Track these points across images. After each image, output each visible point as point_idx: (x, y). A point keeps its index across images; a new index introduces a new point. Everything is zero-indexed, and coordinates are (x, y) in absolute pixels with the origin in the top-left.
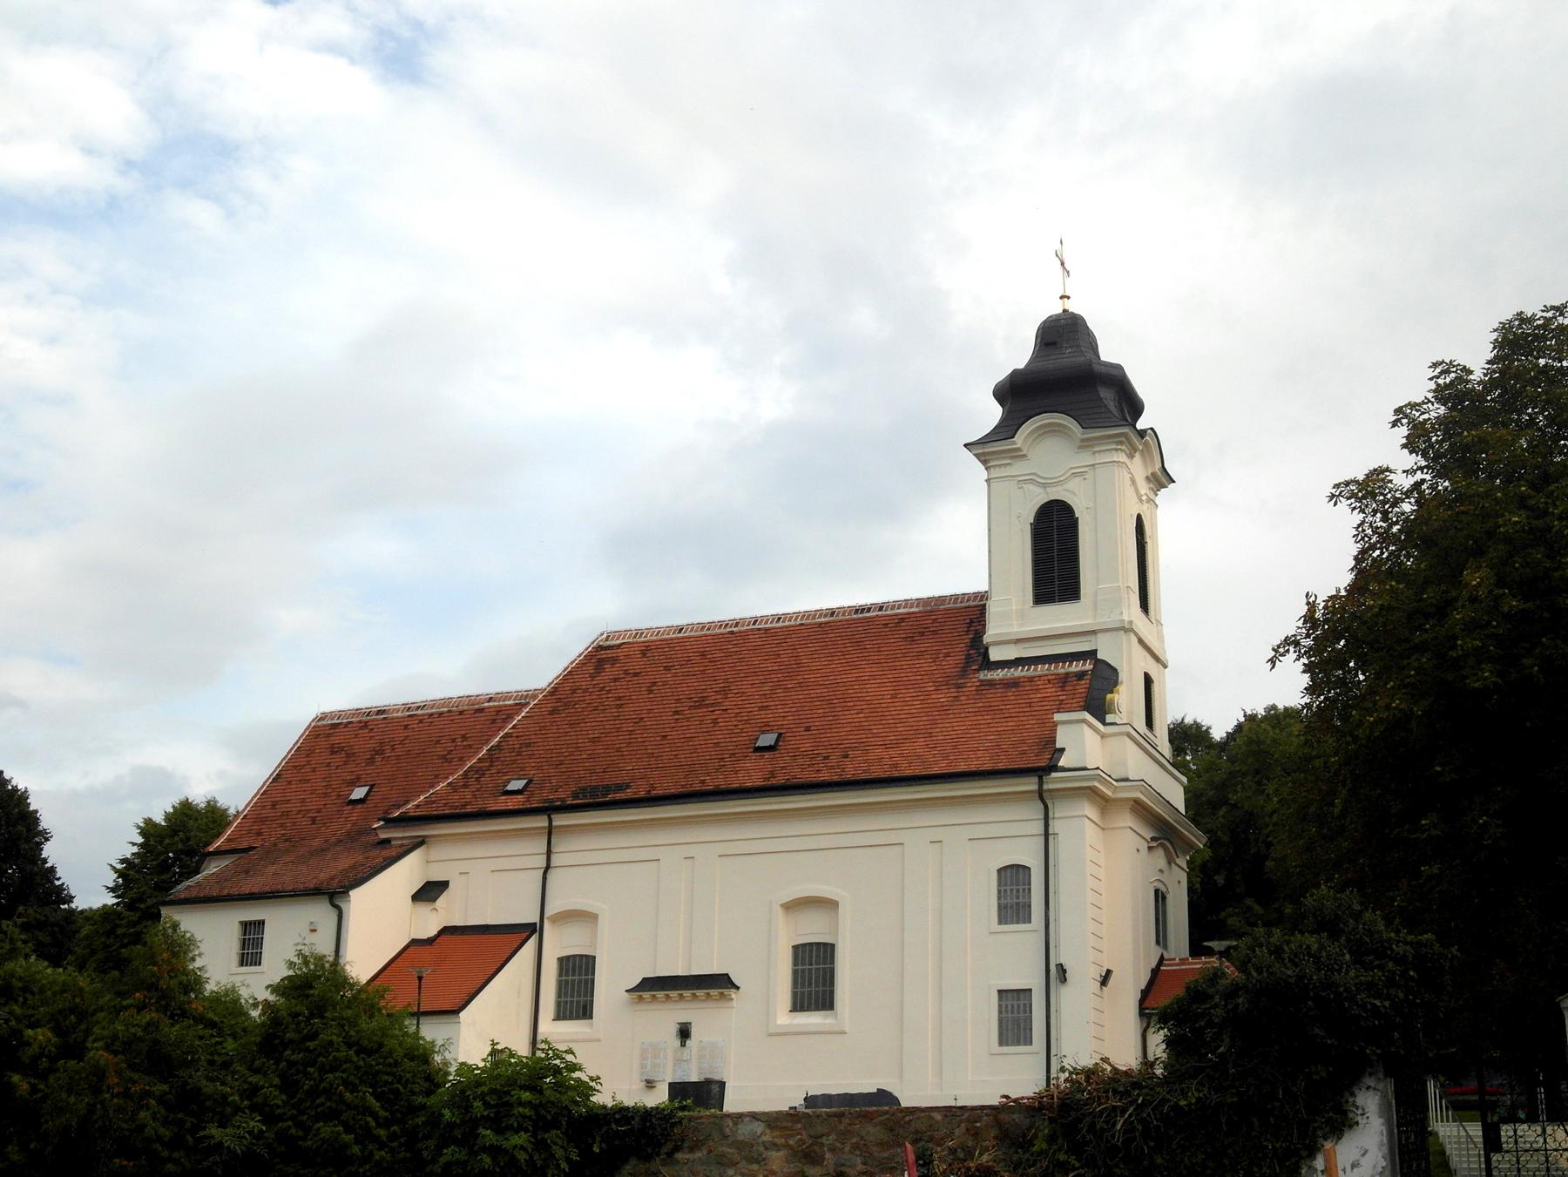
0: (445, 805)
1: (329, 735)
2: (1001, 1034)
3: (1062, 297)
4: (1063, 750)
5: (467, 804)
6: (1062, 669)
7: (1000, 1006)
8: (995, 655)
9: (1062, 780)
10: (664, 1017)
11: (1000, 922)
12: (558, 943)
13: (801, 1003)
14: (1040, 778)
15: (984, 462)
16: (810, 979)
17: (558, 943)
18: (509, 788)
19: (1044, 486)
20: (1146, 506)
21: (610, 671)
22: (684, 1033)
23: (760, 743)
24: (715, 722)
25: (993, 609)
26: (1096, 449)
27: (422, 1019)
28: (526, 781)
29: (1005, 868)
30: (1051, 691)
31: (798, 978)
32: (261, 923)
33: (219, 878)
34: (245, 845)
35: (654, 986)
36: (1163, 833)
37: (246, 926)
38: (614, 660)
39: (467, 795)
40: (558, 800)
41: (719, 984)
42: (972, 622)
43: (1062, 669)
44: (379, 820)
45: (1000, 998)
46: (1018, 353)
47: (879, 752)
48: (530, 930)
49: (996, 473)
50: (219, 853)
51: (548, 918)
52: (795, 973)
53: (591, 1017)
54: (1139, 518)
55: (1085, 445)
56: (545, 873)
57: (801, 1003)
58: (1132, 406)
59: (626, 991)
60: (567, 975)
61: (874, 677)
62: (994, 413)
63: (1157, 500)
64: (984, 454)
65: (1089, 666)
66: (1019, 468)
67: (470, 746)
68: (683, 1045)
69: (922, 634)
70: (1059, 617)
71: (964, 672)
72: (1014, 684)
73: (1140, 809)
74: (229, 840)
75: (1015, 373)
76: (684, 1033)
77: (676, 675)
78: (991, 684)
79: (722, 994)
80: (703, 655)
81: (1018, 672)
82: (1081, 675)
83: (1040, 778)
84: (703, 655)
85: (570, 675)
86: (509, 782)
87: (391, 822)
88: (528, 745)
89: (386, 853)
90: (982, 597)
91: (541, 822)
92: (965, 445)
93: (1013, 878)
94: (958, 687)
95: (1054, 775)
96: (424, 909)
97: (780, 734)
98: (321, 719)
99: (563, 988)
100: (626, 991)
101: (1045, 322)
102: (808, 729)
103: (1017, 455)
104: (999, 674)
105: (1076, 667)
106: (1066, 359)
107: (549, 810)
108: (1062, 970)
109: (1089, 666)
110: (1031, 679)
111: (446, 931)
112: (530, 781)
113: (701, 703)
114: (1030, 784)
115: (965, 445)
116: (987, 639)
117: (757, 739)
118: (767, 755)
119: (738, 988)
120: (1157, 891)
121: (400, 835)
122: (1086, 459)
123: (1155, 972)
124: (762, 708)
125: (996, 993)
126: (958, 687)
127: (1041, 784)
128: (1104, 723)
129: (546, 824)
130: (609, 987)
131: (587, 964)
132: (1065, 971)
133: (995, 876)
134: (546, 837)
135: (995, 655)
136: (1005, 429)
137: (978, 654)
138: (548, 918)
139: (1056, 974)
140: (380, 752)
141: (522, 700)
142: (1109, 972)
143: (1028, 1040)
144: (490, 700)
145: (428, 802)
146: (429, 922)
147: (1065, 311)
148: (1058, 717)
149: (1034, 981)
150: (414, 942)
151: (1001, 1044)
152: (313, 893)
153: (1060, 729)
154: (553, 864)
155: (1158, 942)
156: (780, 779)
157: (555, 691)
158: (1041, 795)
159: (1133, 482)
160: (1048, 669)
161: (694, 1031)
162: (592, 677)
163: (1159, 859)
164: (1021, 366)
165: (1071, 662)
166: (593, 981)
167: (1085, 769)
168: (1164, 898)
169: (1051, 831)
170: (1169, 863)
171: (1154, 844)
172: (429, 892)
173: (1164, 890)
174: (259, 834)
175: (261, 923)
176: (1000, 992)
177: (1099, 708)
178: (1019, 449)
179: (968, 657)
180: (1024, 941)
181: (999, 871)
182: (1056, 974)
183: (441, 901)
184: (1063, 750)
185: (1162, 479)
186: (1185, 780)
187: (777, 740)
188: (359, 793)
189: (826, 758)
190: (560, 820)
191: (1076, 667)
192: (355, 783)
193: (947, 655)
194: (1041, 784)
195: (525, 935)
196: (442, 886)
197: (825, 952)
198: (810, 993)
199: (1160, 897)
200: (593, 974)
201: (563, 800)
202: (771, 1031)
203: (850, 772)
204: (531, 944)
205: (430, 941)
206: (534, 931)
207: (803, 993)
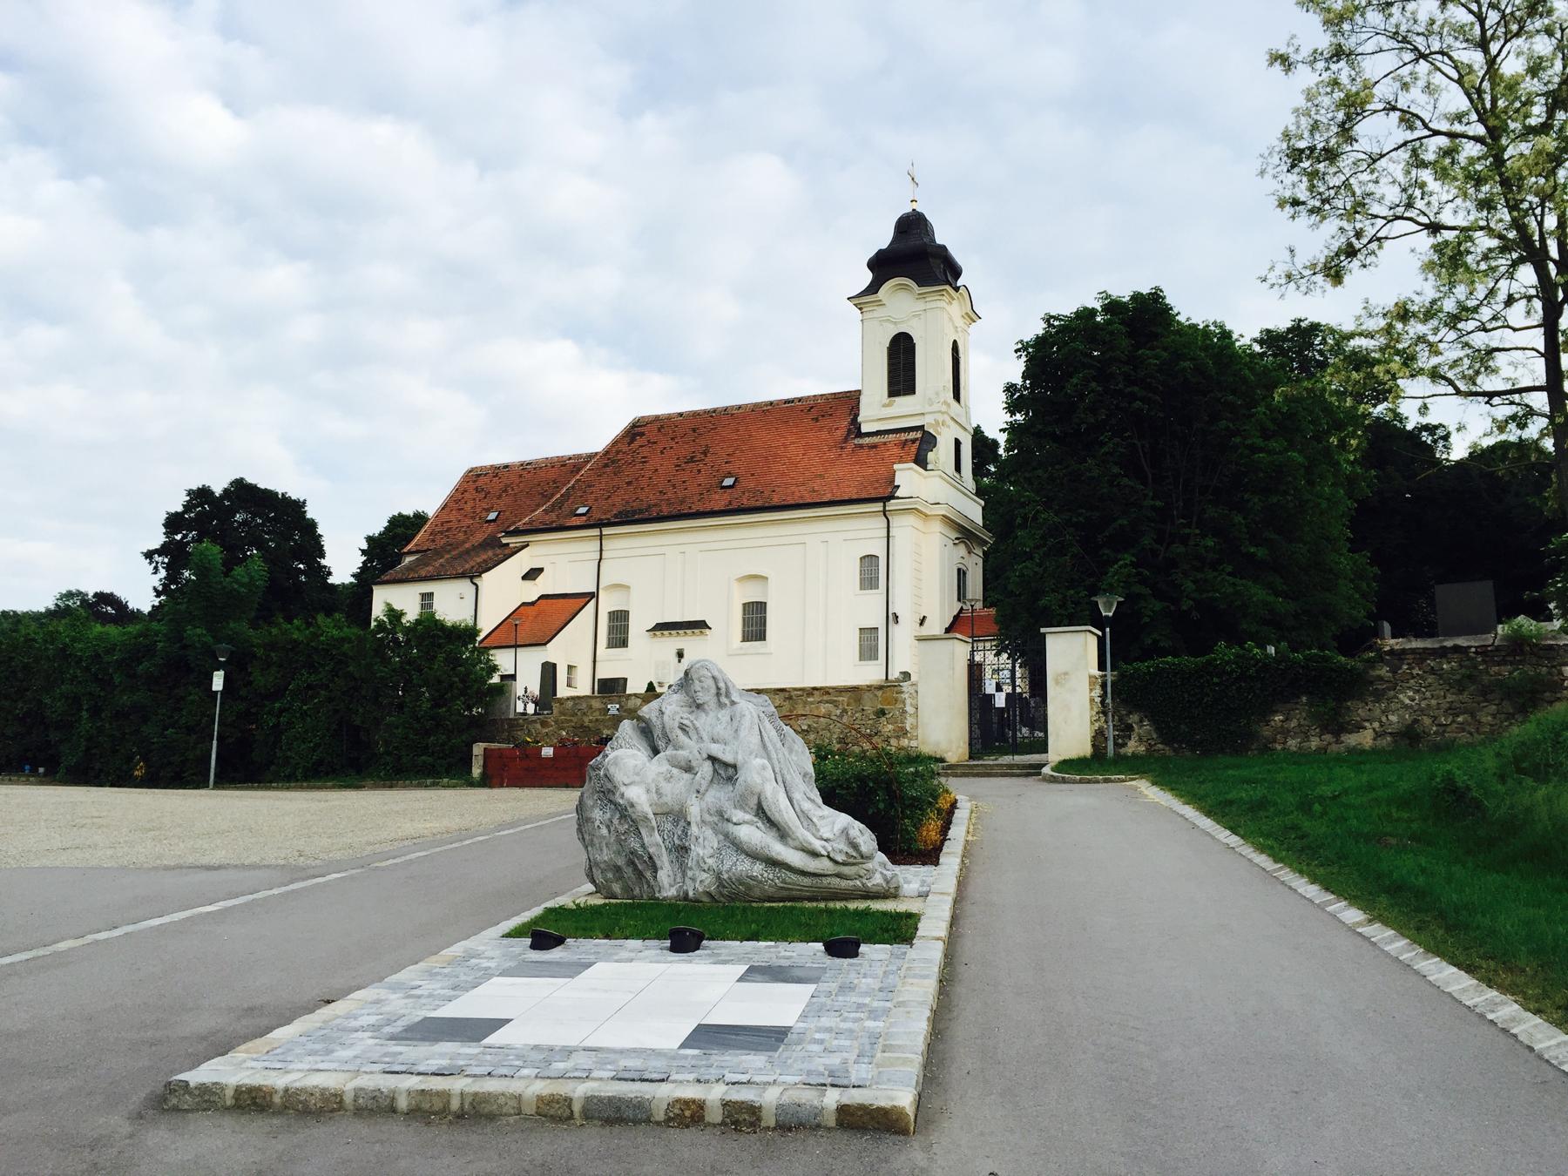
0: (540, 523)
1: (475, 481)
2: (860, 656)
3: (912, 201)
4: (898, 487)
5: (553, 522)
6: (904, 436)
7: (860, 638)
8: (864, 429)
9: (897, 504)
10: (673, 642)
11: (861, 589)
12: (608, 604)
13: (747, 638)
14: (884, 503)
15: (860, 309)
16: (756, 622)
17: (608, 604)
18: (578, 512)
19: (895, 323)
20: (960, 334)
21: (639, 441)
22: (680, 655)
23: (724, 484)
24: (699, 471)
25: (864, 401)
26: (927, 299)
27: (518, 650)
28: (587, 508)
29: (864, 557)
30: (896, 451)
31: (746, 622)
32: (432, 594)
33: (409, 568)
34: (425, 548)
35: (662, 627)
36: (965, 535)
37: (909, 388)
38: (642, 434)
39: (553, 516)
40: (607, 519)
41: (700, 625)
42: (853, 408)
43: (904, 436)
44: (502, 532)
45: (861, 634)
46: (883, 237)
47: (793, 488)
48: (592, 596)
49: (867, 315)
50: (410, 553)
51: (603, 589)
52: (744, 619)
53: (627, 646)
54: (955, 342)
55: (922, 296)
56: (599, 562)
57: (747, 638)
58: (956, 272)
59: (647, 631)
60: (749, 614)
61: (794, 443)
62: (867, 277)
63: (970, 330)
64: (860, 304)
65: (919, 435)
66: (879, 312)
67: (558, 487)
68: (679, 661)
69: (823, 416)
70: (904, 403)
71: (846, 440)
72: (874, 446)
73: (947, 520)
74: (416, 545)
75: (880, 252)
76: (680, 655)
77: (677, 443)
78: (861, 446)
79: (701, 632)
80: (694, 430)
81: (875, 440)
82: (914, 441)
83: (884, 503)
84: (694, 430)
85: (615, 443)
86: (578, 508)
87: (509, 534)
88: (590, 487)
89: (507, 552)
90: (859, 392)
91: (596, 532)
92: (848, 299)
93: (869, 561)
94: (842, 448)
95: (892, 501)
96: (528, 583)
97: (736, 479)
98: (470, 471)
99: (611, 630)
100: (647, 631)
101: (900, 218)
102: (753, 475)
103: (880, 303)
104: (867, 440)
105: (912, 435)
106: (912, 242)
107: (600, 525)
108: (896, 617)
109: (919, 435)
110: (885, 443)
111: (543, 597)
112: (591, 508)
113: (692, 460)
114: (878, 507)
115: (848, 299)
116: (859, 419)
117: (723, 481)
118: (729, 491)
119: (710, 628)
120: (959, 570)
121: (514, 541)
122: (921, 305)
123: (956, 618)
124: (726, 463)
125: (858, 632)
126: (842, 448)
127: (884, 507)
128: (926, 470)
129: (599, 534)
130: (638, 628)
131: (625, 616)
132: (897, 617)
133: (859, 561)
134: (599, 542)
135: (864, 429)
136: (873, 288)
137: (855, 429)
138: (603, 589)
139: (892, 618)
140: (506, 491)
141: (591, 456)
142: (924, 617)
143: (624, 644)
144: (570, 459)
145: (531, 522)
146: (532, 591)
147: (914, 210)
148: (896, 467)
149: (879, 622)
150: (524, 604)
151: (860, 660)
152: (462, 576)
153: (898, 474)
154: (603, 557)
155: (959, 600)
156: (735, 506)
157: (607, 452)
158: (884, 512)
159: (951, 319)
160: (900, 437)
161: (685, 653)
162: (629, 444)
163: (962, 550)
164: (885, 246)
165: (909, 433)
166: (765, 617)
167: (912, 497)
168: (964, 573)
169: (891, 535)
170: (969, 553)
171: (957, 542)
172: (532, 574)
173: (965, 569)
174: (433, 541)
175: (432, 594)
176: (860, 629)
177: (921, 461)
178: (880, 300)
179: (849, 430)
180: (876, 598)
181: (861, 559)
182: (892, 618)
183: (540, 578)
184: (898, 487)
185: (973, 316)
186: (983, 503)
187: (735, 482)
188: (492, 516)
189: (762, 492)
190: (606, 531)
191: (912, 435)
192: (488, 510)
193: (837, 429)
194: (884, 507)
195: (587, 599)
196: (526, 577)
197: (761, 607)
198: (752, 631)
199: (961, 574)
200: (765, 613)
201: (608, 519)
202: (731, 653)
203: (776, 501)
204: (593, 602)
205: (533, 604)
206: (594, 597)
207: (748, 631)
